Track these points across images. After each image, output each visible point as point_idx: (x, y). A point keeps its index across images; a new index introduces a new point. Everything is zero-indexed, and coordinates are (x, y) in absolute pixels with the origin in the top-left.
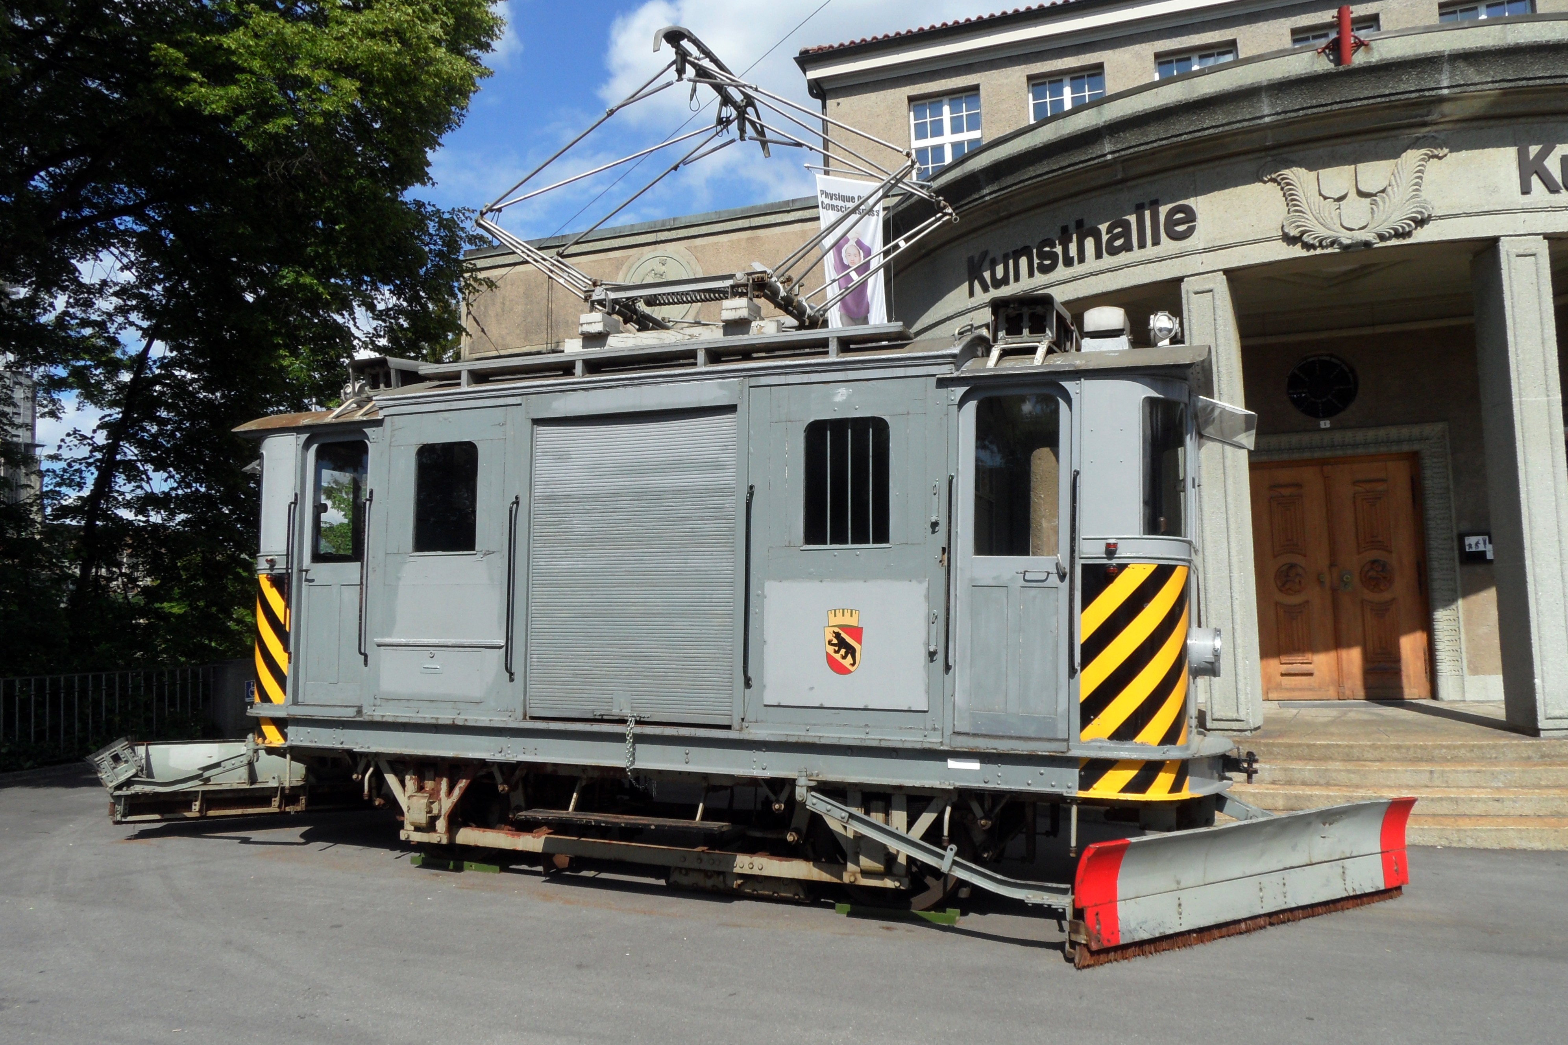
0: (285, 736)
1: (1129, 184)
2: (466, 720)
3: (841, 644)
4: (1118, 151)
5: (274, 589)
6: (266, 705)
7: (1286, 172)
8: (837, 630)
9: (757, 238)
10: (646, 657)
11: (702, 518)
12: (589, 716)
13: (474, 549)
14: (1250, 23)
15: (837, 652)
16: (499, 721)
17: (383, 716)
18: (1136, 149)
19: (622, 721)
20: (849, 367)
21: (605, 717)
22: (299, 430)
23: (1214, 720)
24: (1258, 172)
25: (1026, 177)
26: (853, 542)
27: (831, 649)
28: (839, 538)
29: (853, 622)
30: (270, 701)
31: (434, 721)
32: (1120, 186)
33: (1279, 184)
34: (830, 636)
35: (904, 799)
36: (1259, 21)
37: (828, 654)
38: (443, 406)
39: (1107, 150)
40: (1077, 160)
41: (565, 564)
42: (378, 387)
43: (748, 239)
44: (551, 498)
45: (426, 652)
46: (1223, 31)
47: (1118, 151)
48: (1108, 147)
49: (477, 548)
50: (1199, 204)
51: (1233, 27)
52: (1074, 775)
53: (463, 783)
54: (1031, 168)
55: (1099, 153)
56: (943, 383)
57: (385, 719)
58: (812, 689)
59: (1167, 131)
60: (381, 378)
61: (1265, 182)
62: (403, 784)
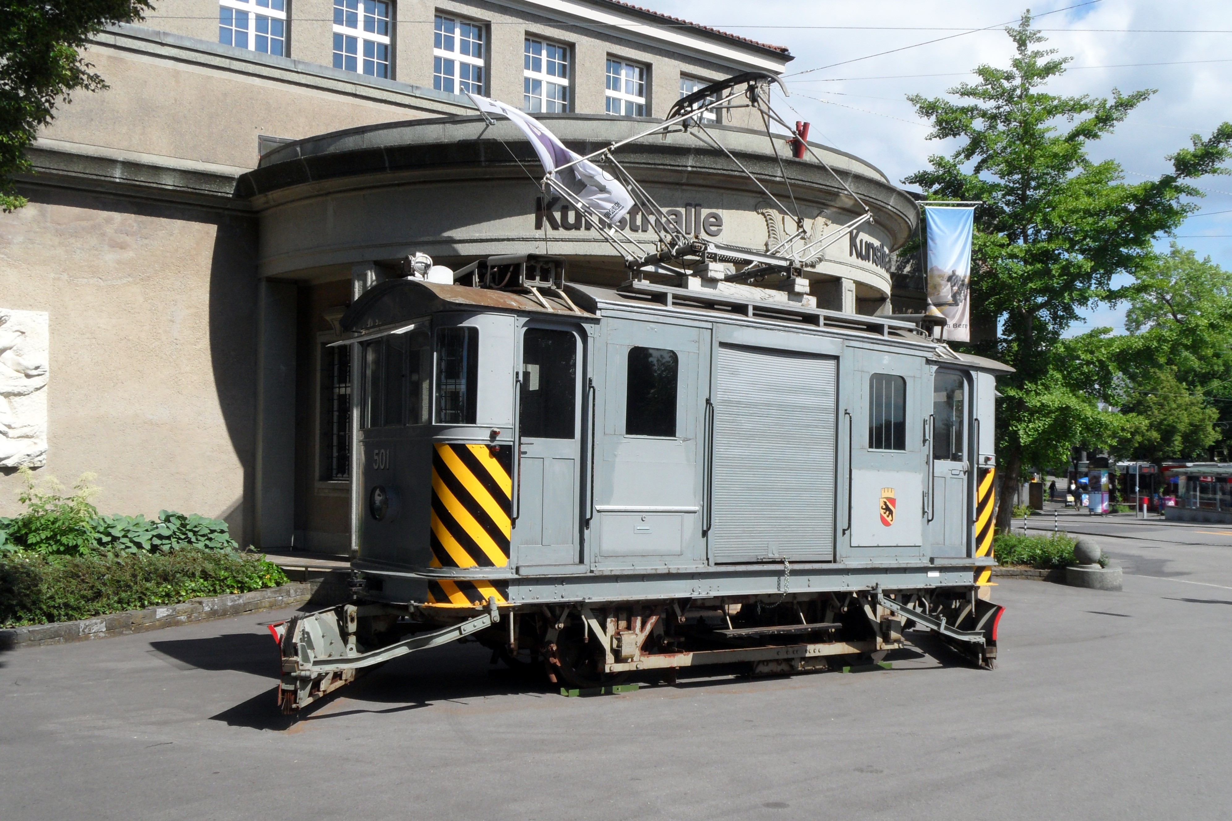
0: (506, 597)
1: (684, 187)
2: (678, 569)
3: (887, 509)
4: (696, 167)
5: (494, 460)
6: (487, 569)
7: (770, 210)
8: (885, 500)
9: (121, 60)
10: (786, 518)
11: (816, 427)
12: (754, 560)
13: (675, 436)
14: (501, 13)
15: (885, 513)
16: (692, 568)
17: (611, 571)
18: (707, 170)
19: (782, 562)
20: (893, 344)
21: (764, 560)
22: (520, 313)
23: (581, 561)
24: (756, 206)
25: (627, 160)
26: (895, 449)
27: (882, 511)
28: (888, 447)
29: (891, 495)
30: (492, 564)
31: (653, 572)
32: (678, 187)
33: (765, 217)
34: (882, 504)
35: (901, 597)
36: (507, 15)
37: (881, 515)
38: (662, 319)
39: (690, 164)
40: (667, 162)
41: (736, 452)
42: (534, 279)
43: (109, 57)
44: (727, 402)
45: (638, 516)
46: (484, 11)
47: (696, 167)
48: (690, 162)
49: (677, 435)
50: (725, 214)
51: (491, 11)
52: (971, 574)
53: (654, 619)
54: (632, 156)
55: (684, 164)
56: (929, 362)
57: (613, 573)
58: (873, 535)
59: (728, 166)
60: (553, 274)
61: (758, 213)
62: (604, 627)
